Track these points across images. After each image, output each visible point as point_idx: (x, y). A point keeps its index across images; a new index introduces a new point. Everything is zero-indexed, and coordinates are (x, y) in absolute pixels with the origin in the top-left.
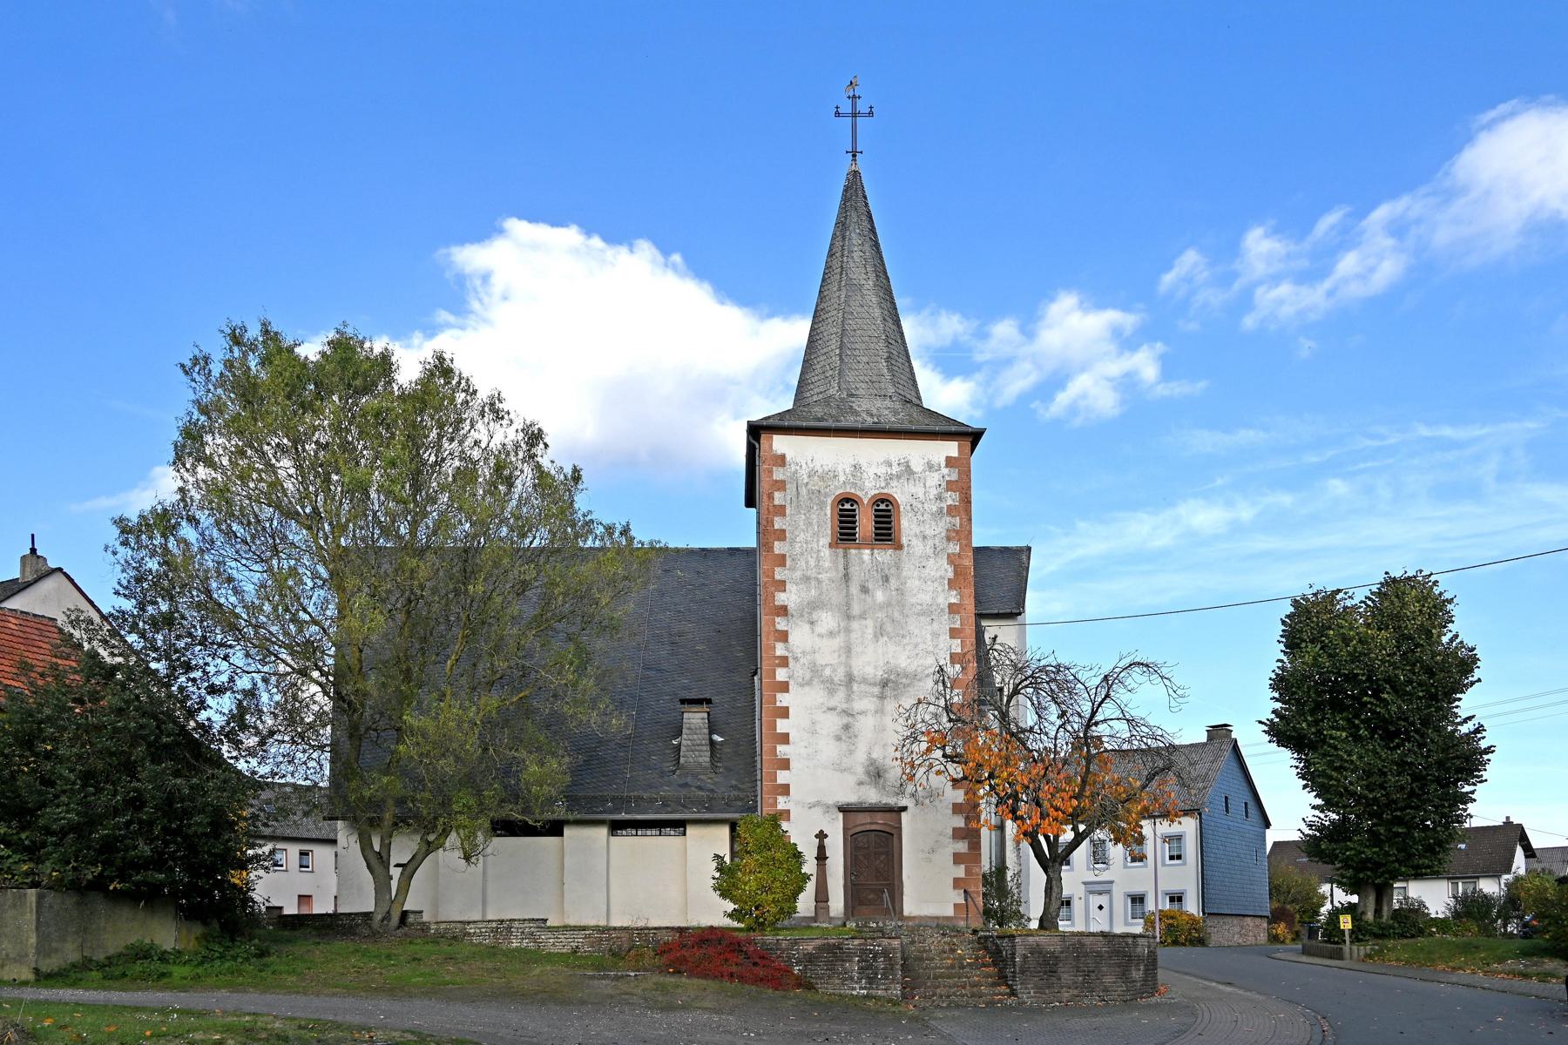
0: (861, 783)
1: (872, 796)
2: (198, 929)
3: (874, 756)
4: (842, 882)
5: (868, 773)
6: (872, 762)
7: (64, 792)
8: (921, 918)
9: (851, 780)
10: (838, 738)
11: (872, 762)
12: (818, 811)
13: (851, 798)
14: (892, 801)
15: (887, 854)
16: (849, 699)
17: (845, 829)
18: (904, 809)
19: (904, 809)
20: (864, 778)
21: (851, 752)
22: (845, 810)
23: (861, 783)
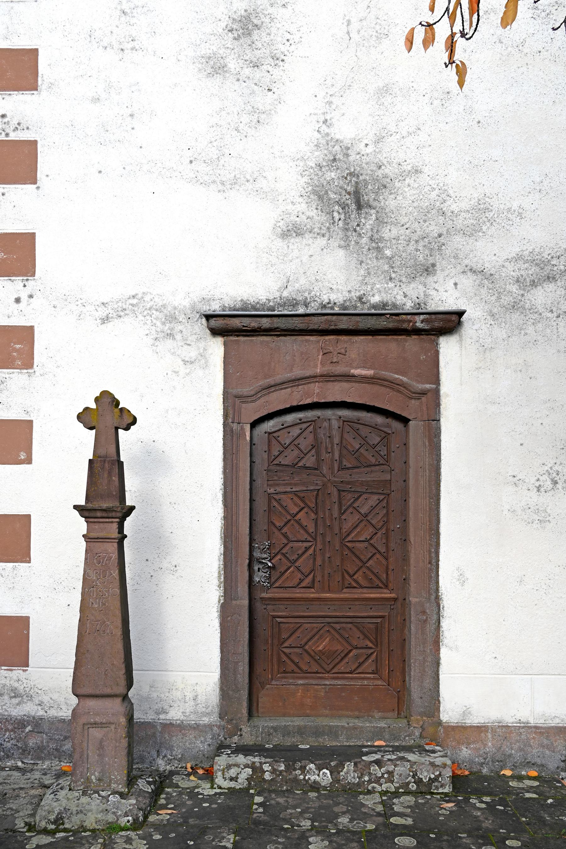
0: (292, 231)
1: (331, 277)
2: (214, 718)
3: (344, 131)
4: (213, 594)
5: (320, 194)
6: (337, 156)
7: (406, 736)
8: (504, 731)
9: (258, 219)
10: (216, 68)
11: (337, 156)
12: (132, 333)
13: (255, 284)
14: (403, 295)
15: (384, 489)
16: (298, 568)
17: (232, 401)
18: (449, 323)
19: (449, 323)
20: (306, 211)
21: (259, 117)
22: (230, 326)
23: (292, 231)
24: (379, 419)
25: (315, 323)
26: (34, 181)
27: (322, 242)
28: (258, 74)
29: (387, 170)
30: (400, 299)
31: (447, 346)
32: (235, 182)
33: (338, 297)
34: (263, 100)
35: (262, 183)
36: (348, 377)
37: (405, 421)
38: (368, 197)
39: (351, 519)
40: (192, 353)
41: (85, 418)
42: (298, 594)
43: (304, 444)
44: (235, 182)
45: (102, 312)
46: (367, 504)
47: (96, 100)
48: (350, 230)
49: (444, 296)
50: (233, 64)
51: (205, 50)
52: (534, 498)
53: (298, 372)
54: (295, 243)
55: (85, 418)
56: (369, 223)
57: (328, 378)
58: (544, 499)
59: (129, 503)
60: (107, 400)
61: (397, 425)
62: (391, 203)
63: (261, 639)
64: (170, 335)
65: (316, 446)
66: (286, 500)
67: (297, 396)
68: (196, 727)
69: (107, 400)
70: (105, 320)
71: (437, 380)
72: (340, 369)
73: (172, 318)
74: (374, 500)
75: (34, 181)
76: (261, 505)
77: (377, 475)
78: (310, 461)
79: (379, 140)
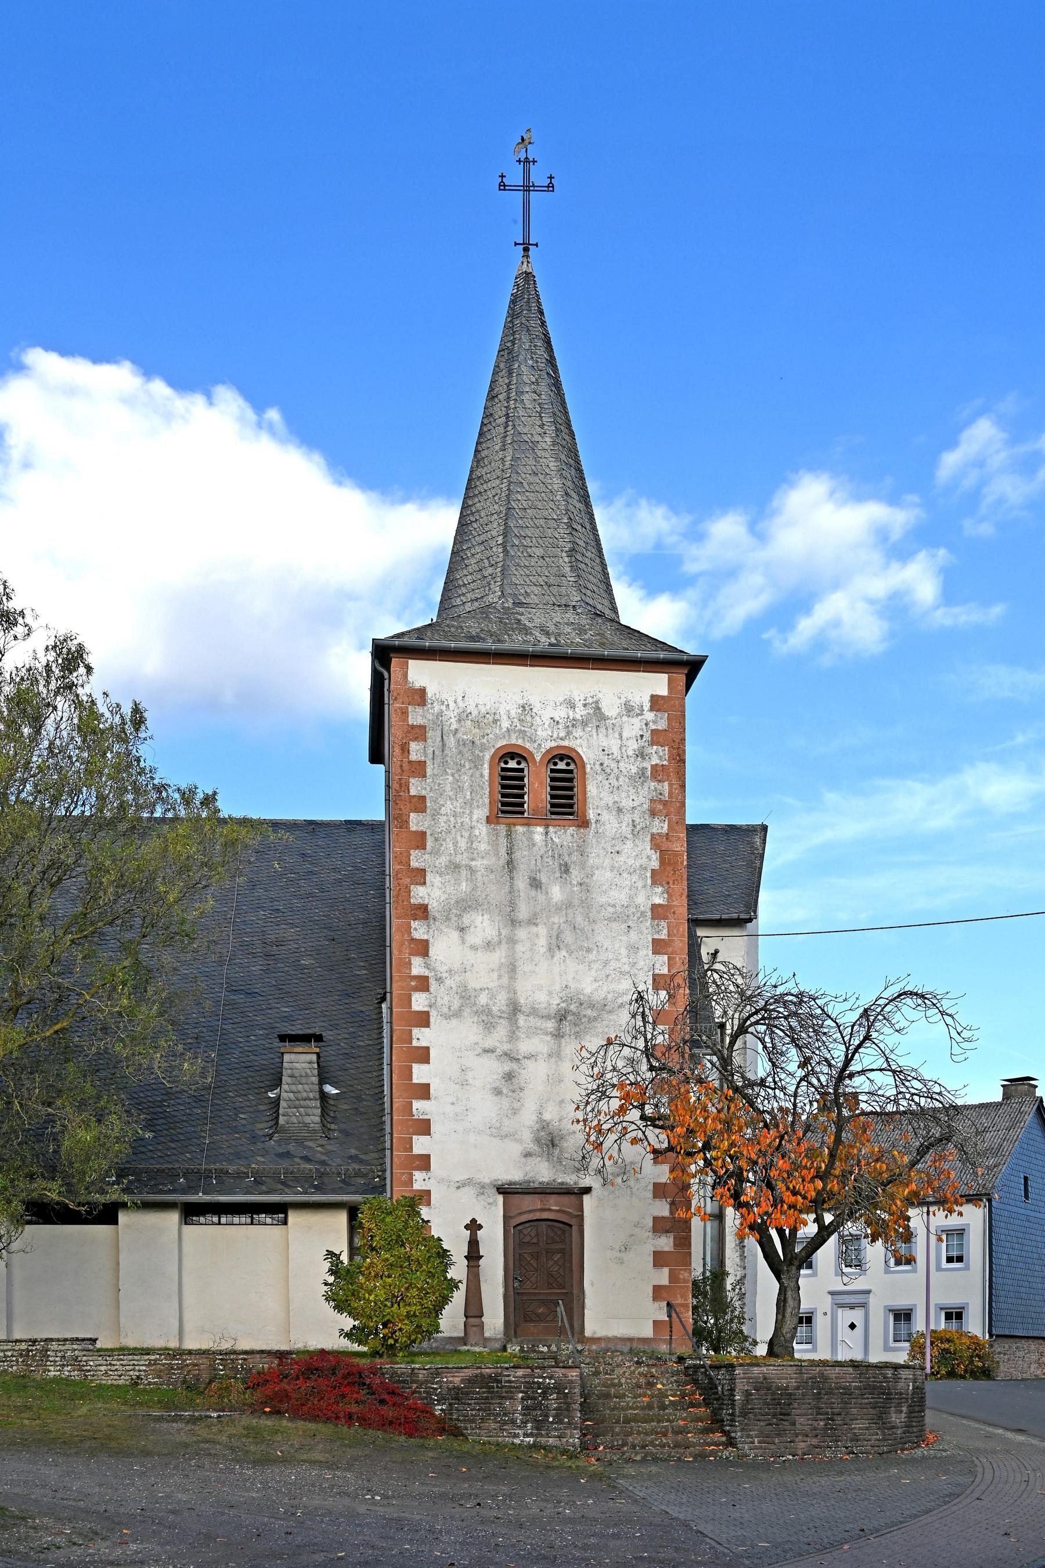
0: (528, 1155)
1: (543, 1173)
2: (501, 1336)
3: (547, 1116)
5: (538, 1140)
9: (515, 1150)
10: (498, 1092)
12: (469, 1193)
14: (570, 1179)
18: (588, 1190)
20: (532, 1147)
21: (515, 1112)
23: (528, 1155)
24: (561, 1225)
25: (539, 1190)
26: (429, 1134)
27: (539, 1159)
28: (514, 1095)
29: (563, 1132)
30: (569, 1181)
31: (586, 1198)
32: (506, 1136)
33: (545, 1180)
34: (517, 1105)
35: (516, 1136)
36: (550, 1210)
37: (571, 1226)
38: (557, 1142)
39: (551, 1263)
40: (491, 1201)
41: (467, 1227)
42: (531, 1291)
43: (533, 1234)
44: (506, 1136)
45: (457, 1185)
46: (557, 1257)
47: (453, 1104)
48: (549, 1154)
49: (586, 1181)
50: (505, 1091)
51: (494, 1085)
52: (618, 1255)
53: (531, 1208)
54: (529, 1159)
55: (467, 1227)
56: (557, 1152)
57: (542, 1210)
58: (622, 1255)
59: (805, 1306)
60: (474, 1221)
61: (567, 1227)
62: (565, 1145)
63: (521, 1309)
64: (483, 1194)
65: (537, 1235)
66: (526, 1255)
67: (530, 1217)
68: (495, 1339)
69: (474, 1221)
70: (458, 1188)
71: (582, 1211)
72: (547, 1207)
73: (483, 1187)
74: (559, 1256)
75: (429, 1134)
76: (517, 1257)
77: (561, 1246)
78: (535, 1241)
79: (560, 1120)
